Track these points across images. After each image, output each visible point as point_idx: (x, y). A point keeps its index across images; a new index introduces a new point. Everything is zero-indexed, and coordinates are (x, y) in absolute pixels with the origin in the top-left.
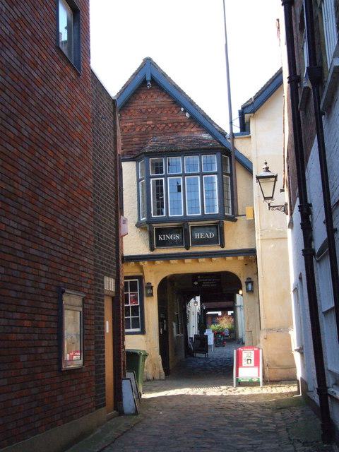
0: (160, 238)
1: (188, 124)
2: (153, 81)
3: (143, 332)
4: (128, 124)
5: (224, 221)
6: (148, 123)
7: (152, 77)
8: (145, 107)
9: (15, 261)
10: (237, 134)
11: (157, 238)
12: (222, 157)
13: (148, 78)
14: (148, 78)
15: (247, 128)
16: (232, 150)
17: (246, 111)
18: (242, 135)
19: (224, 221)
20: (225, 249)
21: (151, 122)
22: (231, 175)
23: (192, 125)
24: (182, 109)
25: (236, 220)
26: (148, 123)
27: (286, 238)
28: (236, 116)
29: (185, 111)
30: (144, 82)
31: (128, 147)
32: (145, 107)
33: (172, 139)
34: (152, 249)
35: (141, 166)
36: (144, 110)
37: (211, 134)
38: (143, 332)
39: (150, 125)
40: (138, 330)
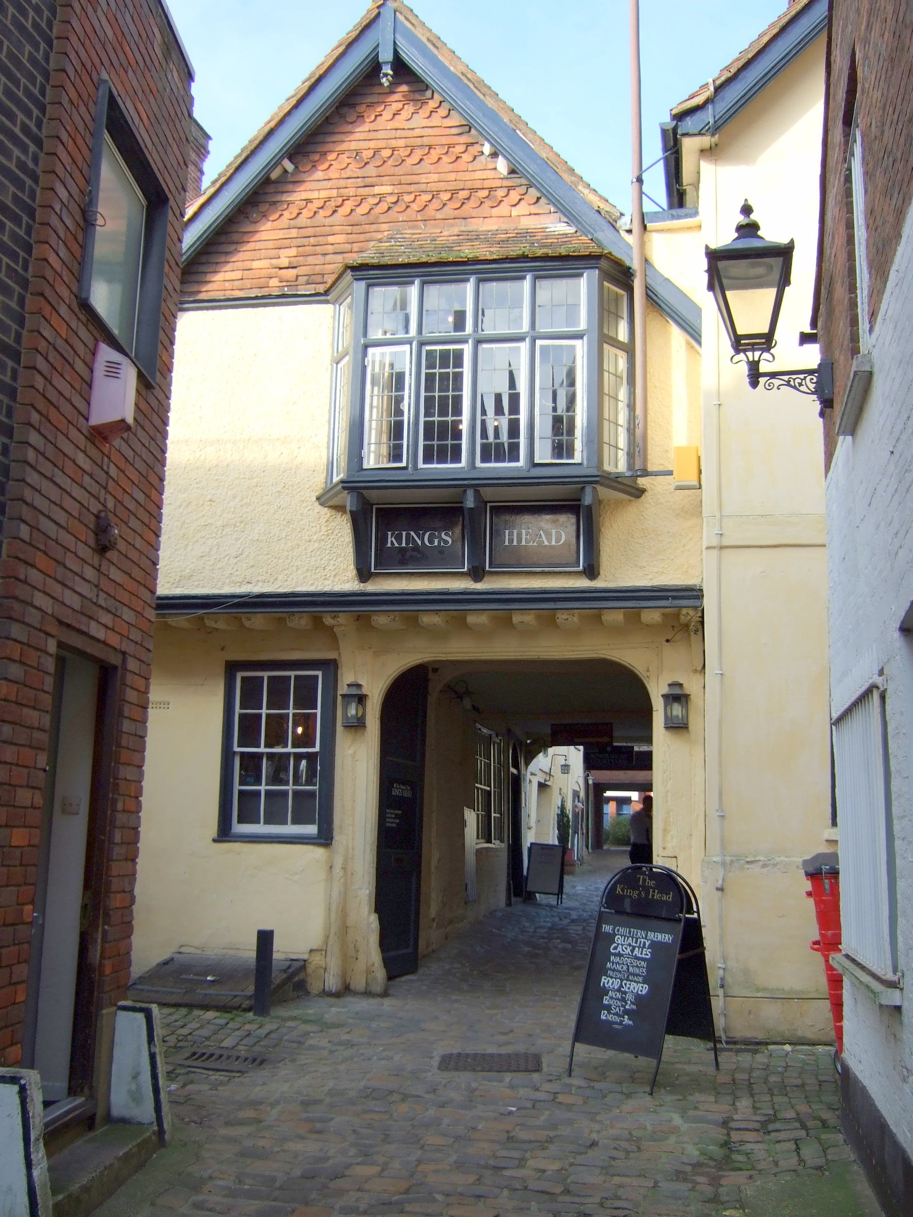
0: (391, 540)
1: (501, 193)
2: (402, 69)
3: (325, 838)
4: (315, 195)
5: (556, 843)
6: (377, 190)
7: (396, 53)
8: (372, 144)
9: (70, 575)
10: (656, 217)
11: (382, 540)
12: (601, 287)
13: (386, 56)
14: (386, 56)
15: (689, 198)
16: (635, 264)
17: (689, 124)
18: (673, 217)
19: (556, 843)
20: (599, 584)
21: (388, 189)
22: (629, 349)
23: (514, 196)
24: (487, 149)
25: (639, 493)
26: (377, 190)
27: (540, 389)
28: (654, 150)
29: (494, 155)
30: (373, 69)
31: (311, 260)
32: (372, 144)
33: (447, 233)
34: (364, 574)
35: (348, 316)
36: (367, 154)
37: (570, 217)
38: (325, 838)
39: (381, 197)
40: (311, 829)
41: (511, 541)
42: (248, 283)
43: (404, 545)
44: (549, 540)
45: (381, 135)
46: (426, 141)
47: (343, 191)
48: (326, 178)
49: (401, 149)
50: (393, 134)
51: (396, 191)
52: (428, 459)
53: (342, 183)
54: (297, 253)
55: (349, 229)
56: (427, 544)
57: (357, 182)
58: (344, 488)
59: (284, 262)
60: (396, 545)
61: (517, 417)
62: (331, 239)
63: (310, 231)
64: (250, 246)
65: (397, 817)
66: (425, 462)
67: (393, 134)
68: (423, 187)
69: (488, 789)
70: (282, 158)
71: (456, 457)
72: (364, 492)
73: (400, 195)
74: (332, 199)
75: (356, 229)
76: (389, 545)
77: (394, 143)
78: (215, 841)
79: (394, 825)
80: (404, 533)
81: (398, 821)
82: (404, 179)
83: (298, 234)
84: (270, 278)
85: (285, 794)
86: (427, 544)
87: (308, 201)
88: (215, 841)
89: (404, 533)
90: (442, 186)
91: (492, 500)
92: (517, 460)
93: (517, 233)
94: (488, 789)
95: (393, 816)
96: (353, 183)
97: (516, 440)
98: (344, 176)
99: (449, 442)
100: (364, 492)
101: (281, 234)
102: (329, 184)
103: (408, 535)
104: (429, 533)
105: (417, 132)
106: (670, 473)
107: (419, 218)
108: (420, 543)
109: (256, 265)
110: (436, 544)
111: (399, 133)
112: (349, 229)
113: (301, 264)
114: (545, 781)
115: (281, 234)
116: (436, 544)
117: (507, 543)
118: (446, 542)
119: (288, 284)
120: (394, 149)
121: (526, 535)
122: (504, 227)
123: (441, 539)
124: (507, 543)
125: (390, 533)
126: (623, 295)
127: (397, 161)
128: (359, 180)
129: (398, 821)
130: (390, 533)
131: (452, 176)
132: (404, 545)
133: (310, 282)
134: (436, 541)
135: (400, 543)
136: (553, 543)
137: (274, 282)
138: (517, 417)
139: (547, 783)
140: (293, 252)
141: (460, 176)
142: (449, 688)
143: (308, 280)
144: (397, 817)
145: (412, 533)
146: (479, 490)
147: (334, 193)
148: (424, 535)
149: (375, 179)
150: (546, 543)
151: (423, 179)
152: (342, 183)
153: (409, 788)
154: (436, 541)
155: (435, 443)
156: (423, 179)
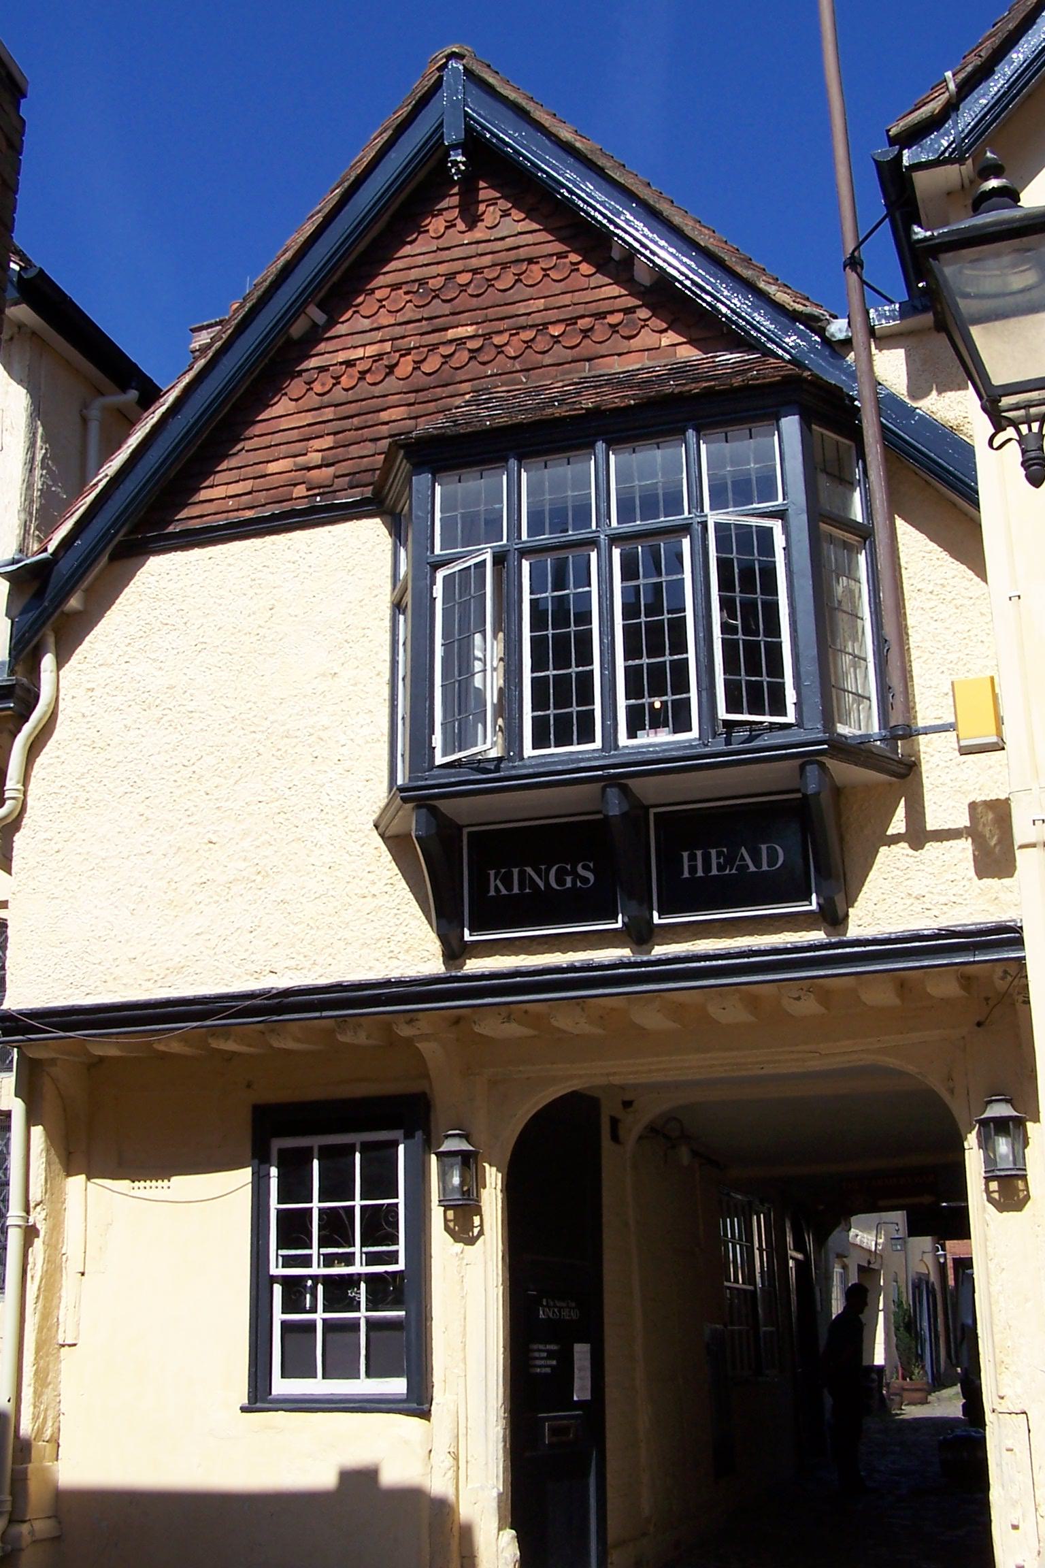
0: (495, 885)
8: (442, 269)
11: (479, 884)
30: (435, 150)
31: (354, 451)
32: (442, 269)
40: (397, 1386)
41: (693, 869)
42: (262, 497)
43: (516, 890)
44: (757, 863)
45: (456, 253)
46: (523, 253)
47: (401, 343)
48: (375, 325)
49: (486, 270)
50: (472, 249)
51: (480, 332)
52: (540, 741)
53: (398, 330)
54: (335, 442)
55: (411, 397)
56: (554, 885)
57: (421, 326)
58: (404, 800)
59: (316, 458)
60: (504, 892)
61: (684, 656)
62: (384, 416)
63: (352, 409)
64: (257, 429)
65: (551, 1355)
66: (535, 746)
67: (472, 249)
68: (522, 321)
69: (751, 1288)
70: (305, 304)
71: (587, 736)
72: (441, 804)
73: (487, 336)
74: (385, 357)
75: (422, 396)
76: (492, 893)
77: (475, 263)
78: (244, 1409)
79: (548, 1370)
80: (516, 871)
81: (554, 1362)
82: (492, 313)
83: (335, 414)
84: (295, 485)
85: (354, 1326)
86: (554, 885)
87: (349, 364)
88: (244, 1409)
89: (516, 871)
90: (552, 315)
91: (657, 802)
92: (689, 729)
93: (669, 369)
94: (751, 1288)
95: (545, 1355)
96: (415, 328)
97: (684, 696)
98: (402, 320)
99: (575, 709)
100: (441, 804)
101: (309, 418)
102: (379, 335)
103: (522, 874)
104: (555, 868)
105: (510, 242)
106: (966, 751)
107: (518, 367)
108: (542, 885)
109: (273, 467)
110: (569, 885)
111: (482, 248)
112: (411, 397)
113: (341, 458)
114: (869, 1263)
115: (309, 418)
116: (569, 885)
117: (686, 875)
118: (585, 880)
119: (321, 490)
120: (475, 271)
121: (718, 857)
122: (648, 364)
123: (576, 875)
124: (686, 875)
125: (492, 873)
126: (850, 447)
127: (480, 287)
128: (424, 322)
129: (554, 1362)
130: (492, 873)
131: (566, 300)
132: (516, 890)
133: (355, 483)
134: (569, 879)
135: (509, 887)
136: (765, 868)
137: (300, 491)
138: (684, 656)
139: (871, 1266)
140: (328, 442)
141: (578, 297)
142: (654, 1131)
143: (350, 481)
144: (551, 1355)
145: (529, 870)
146: (626, 785)
147: (387, 346)
148: (548, 871)
149: (451, 317)
150: (752, 868)
151: (521, 308)
152: (398, 330)
153: (573, 1305)
154: (569, 879)
155: (551, 712)
156: (521, 308)
